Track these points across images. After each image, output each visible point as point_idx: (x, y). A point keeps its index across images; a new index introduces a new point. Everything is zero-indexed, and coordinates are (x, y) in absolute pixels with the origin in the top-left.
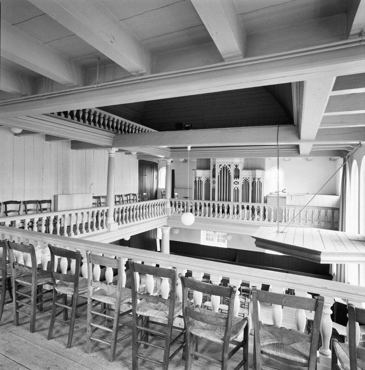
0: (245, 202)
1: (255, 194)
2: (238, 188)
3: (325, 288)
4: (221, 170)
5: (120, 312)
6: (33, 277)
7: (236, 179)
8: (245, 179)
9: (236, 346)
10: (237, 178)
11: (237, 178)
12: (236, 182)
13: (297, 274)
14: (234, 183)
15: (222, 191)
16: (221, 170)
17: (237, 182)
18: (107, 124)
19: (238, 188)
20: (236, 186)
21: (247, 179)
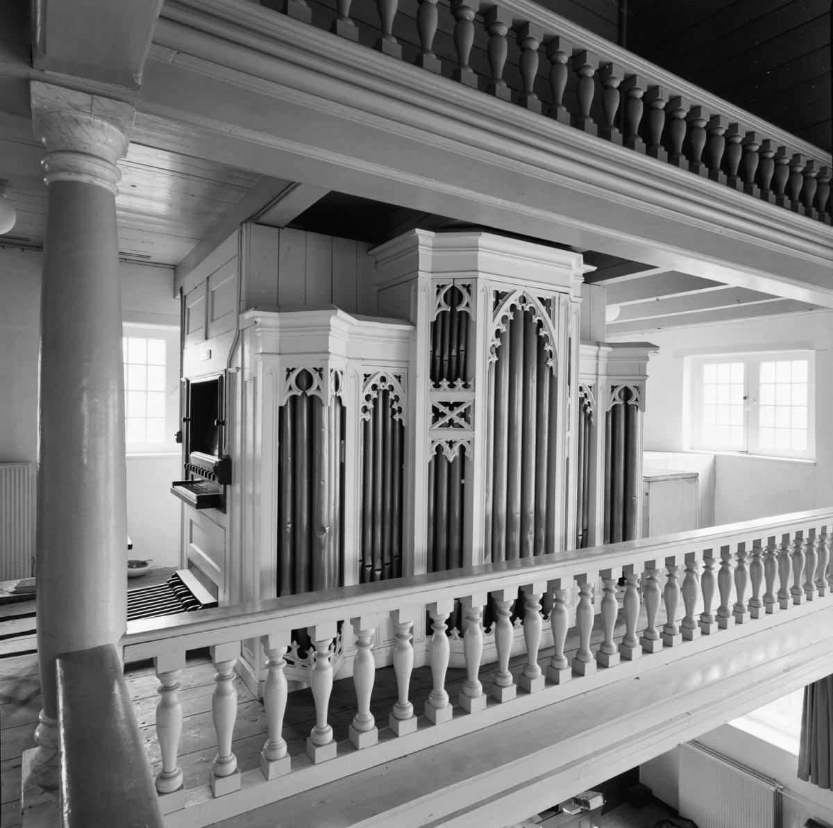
0: (128, 596)
1: (222, 399)
2: (462, 449)
3: (343, 410)
4: (498, 343)
5: (117, 212)
6: (482, 649)
7: (452, 386)
8: (513, 307)
9: (418, 231)
10: (459, 383)
11: (459, 383)
12: (452, 406)
13: (515, 238)
14: (437, 414)
15: (543, 448)
16: (498, 343)
17: (458, 404)
18: (772, 180)
19: (462, 449)
20: (451, 434)
21: (392, 388)
